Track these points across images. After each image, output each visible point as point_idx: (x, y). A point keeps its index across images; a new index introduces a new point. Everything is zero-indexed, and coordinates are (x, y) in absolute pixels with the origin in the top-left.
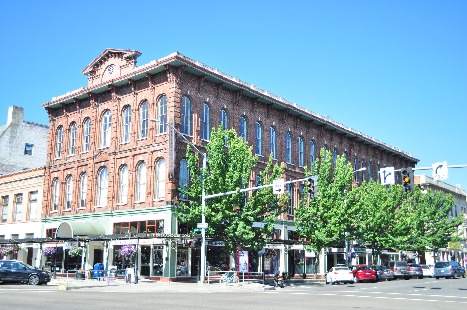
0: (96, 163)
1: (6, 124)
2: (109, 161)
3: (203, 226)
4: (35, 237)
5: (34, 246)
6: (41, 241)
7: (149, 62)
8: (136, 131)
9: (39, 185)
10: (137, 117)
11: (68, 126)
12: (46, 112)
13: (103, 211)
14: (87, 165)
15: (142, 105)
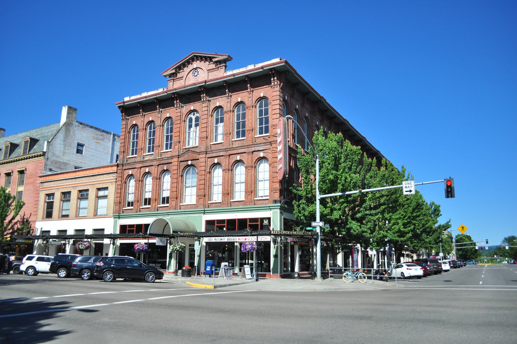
0: (181, 162)
1: (59, 122)
2: (198, 159)
3: (318, 224)
4: (106, 232)
5: (106, 241)
6: (113, 237)
7: (246, 66)
8: (231, 131)
9: (110, 182)
10: (232, 118)
11: (145, 126)
12: (119, 111)
13: (195, 208)
15: (258, 101)
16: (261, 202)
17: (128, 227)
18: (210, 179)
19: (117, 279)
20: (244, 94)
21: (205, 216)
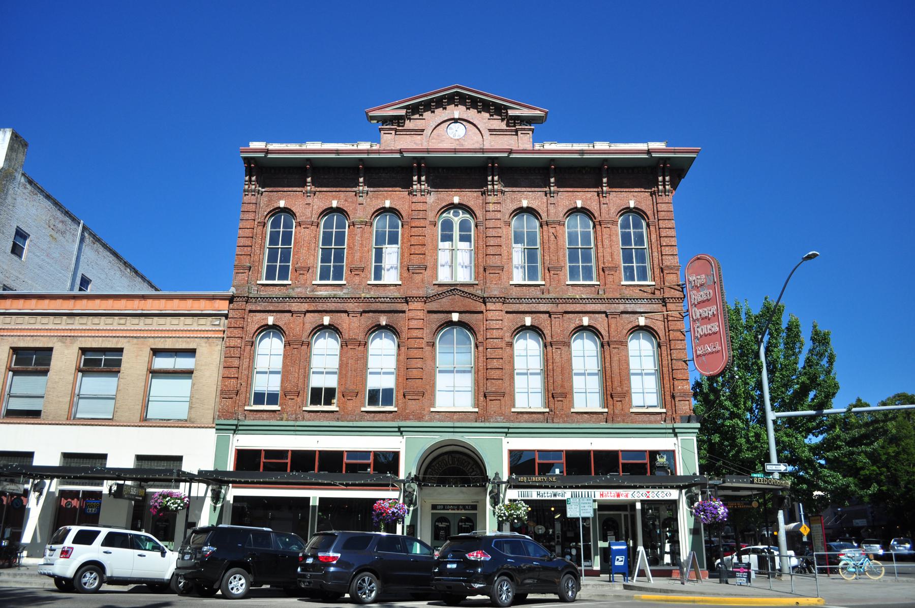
4: (110, 464)
14: (404, 312)
15: (325, 216)
16: (645, 418)
17: (263, 454)
18: (252, 358)
19: (530, 596)
20: (589, 195)
21: (237, 437)
